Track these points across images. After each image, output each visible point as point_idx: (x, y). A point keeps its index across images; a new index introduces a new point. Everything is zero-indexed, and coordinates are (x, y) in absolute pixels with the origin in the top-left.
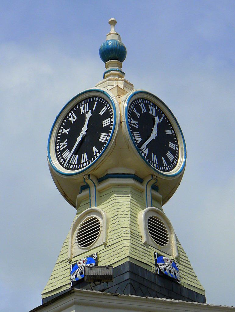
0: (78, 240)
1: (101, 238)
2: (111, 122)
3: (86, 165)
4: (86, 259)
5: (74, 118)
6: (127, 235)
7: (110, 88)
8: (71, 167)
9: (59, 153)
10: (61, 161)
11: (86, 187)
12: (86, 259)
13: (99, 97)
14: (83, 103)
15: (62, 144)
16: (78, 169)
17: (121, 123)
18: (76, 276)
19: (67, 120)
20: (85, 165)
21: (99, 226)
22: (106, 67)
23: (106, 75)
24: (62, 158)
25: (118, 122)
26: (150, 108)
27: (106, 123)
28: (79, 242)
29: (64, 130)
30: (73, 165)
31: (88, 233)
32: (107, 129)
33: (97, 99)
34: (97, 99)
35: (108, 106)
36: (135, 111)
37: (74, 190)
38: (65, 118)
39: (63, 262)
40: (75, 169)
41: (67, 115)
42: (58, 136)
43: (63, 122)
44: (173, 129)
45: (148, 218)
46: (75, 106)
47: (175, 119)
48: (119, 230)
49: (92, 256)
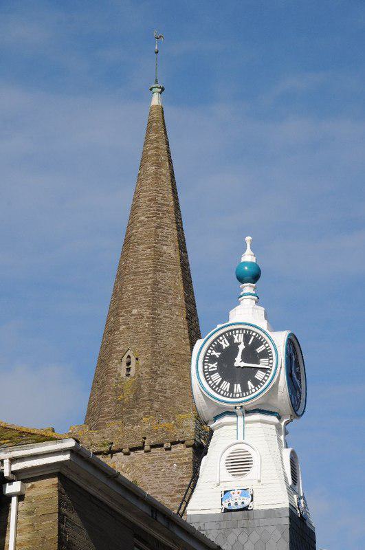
0: (227, 463)
15: (211, 366)
20: (238, 395)
29: (213, 351)
33: (254, 334)
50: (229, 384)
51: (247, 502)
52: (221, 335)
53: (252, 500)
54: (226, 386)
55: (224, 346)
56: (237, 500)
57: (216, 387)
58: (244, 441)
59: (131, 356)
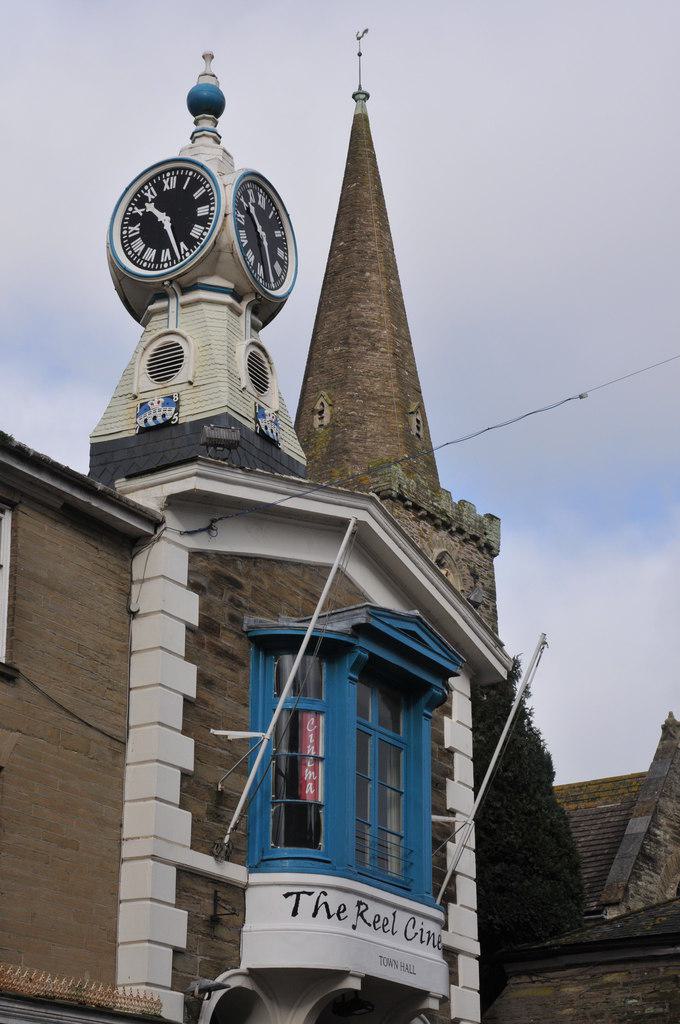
0: (150, 369)
1: (181, 376)
2: (210, 212)
3: (169, 267)
4: (162, 400)
5: (152, 193)
6: (223, 375)
7: (206, 155)
8: (145, 265)
9: (127, 242)
10: (130, 253)
11: (164, 296)
12: (162, 400)
13: (194, 171)
14: (168, 174)
15: (132, 229)
16: (154, 269)
17: (226, 215)
18: (146, 421)
19: (142, 195)
20: (166, 265)
21: (182, 356)
22: (196, 123)
23: (196, 135)
24: (132, 249)
25: (222, 214)
26: (260, 196)
27: (202, 211)
28: (150, 373)
29: (136, 208)
30: (148, 262)
31: (166, 362)
32: (204, 221)
33: (191, 173)
34: (191, 173)
35: (207, 186)
36: (242, 200)
37: (138, 298)
38: (139, 192)
39: (123, 398)
40: (150, 269)
41: (142, 187)
42: (125, 216)
43: (135, 196)
44: (283, 230)
45: (248, 354)
46: (155, 177)
47: (288, 216)
48: (212, 367)
49: (172, 397)
50: (168, 250)
51: (170, 413)
52: (170, 170)
53: (177, 411)
54: (151, 254)
55: (166, 187)
56: (158, 413)
57: (136, 259)
58: (176, 330)
59: (325, 403)
